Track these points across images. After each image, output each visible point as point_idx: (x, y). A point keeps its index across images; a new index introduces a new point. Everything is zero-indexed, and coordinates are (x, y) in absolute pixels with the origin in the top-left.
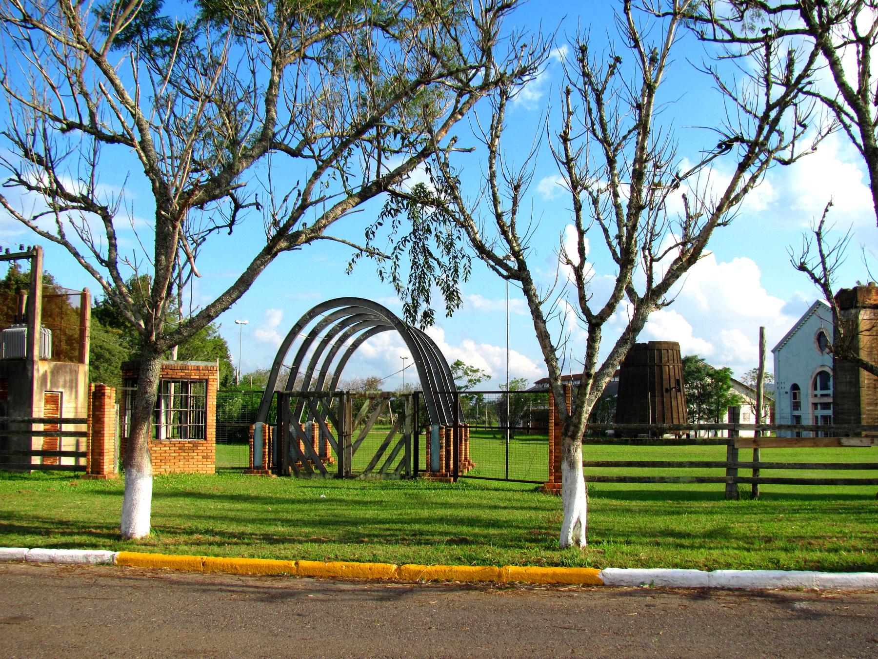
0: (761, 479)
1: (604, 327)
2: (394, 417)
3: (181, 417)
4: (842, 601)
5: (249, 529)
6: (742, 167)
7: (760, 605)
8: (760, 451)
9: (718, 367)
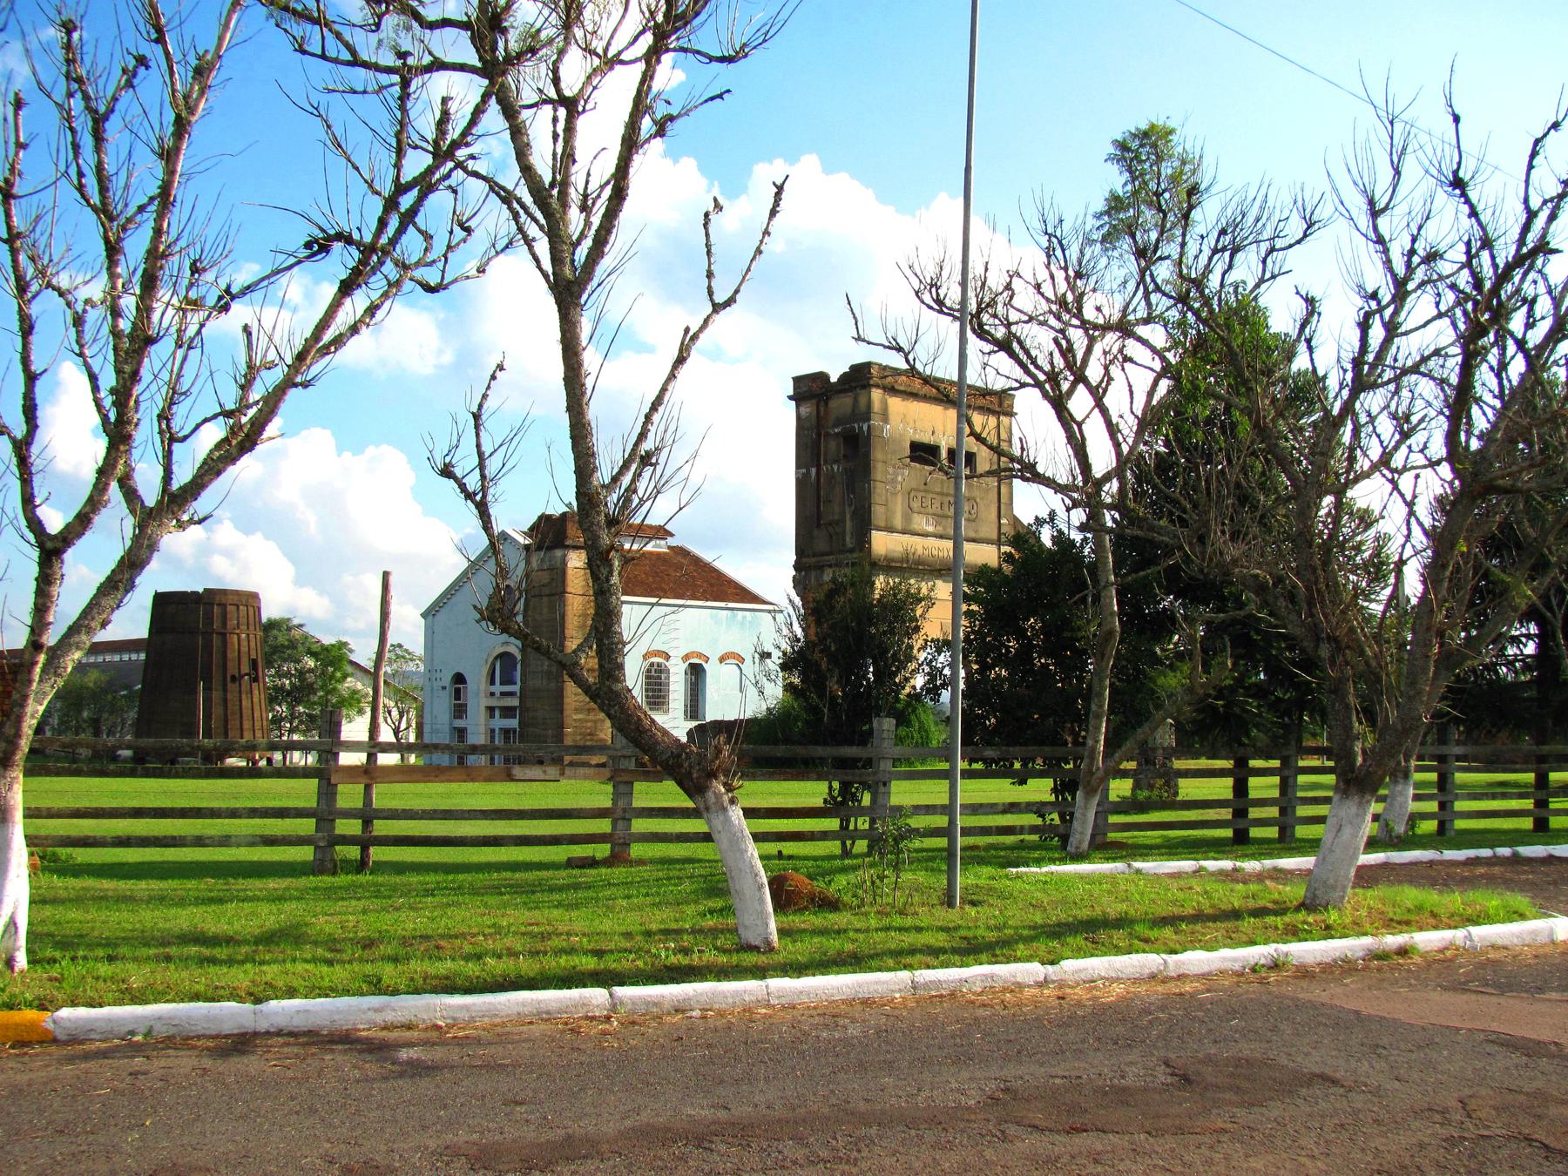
0: (376, 838)
1: (69, 556)
4: (478, 1041)
7: (339, 1058)
8: (375, 789)
9: (328, 640)
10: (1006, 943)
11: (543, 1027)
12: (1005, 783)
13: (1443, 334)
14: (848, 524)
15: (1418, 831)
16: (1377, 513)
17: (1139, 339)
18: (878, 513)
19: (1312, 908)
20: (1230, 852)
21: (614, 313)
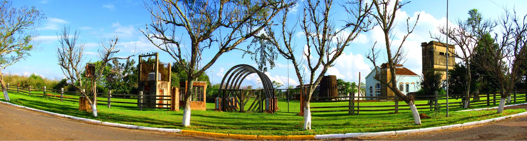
2: (256, 96)
3: (198, 96)
5: (215, 125)
6: (353, 31)
9: (346, 82)
18: (435, 62)
21: (393, 35)
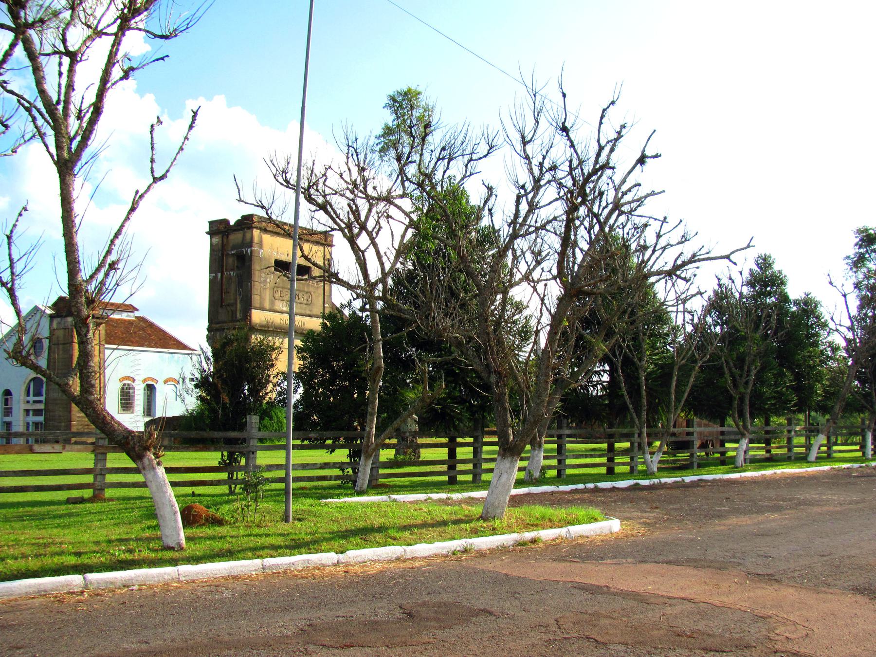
10: (316, 542)
11: (41, 599)
12: (323, 452)
13: (559, 209)
14: (239, 306)
15: (547, 476)
16: (525, 304)
17: (396, 206)
18: (256, 300)
19: (486, 521)
20: (445, 489)
